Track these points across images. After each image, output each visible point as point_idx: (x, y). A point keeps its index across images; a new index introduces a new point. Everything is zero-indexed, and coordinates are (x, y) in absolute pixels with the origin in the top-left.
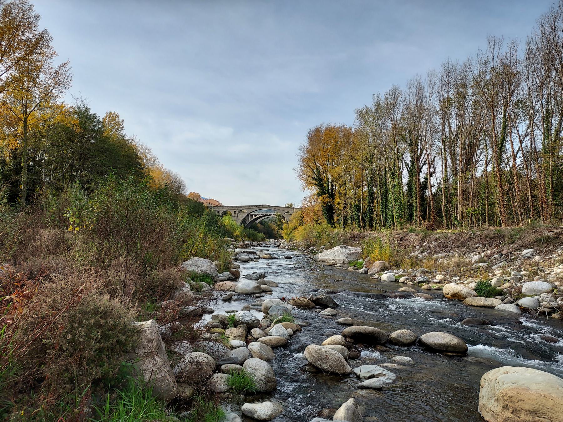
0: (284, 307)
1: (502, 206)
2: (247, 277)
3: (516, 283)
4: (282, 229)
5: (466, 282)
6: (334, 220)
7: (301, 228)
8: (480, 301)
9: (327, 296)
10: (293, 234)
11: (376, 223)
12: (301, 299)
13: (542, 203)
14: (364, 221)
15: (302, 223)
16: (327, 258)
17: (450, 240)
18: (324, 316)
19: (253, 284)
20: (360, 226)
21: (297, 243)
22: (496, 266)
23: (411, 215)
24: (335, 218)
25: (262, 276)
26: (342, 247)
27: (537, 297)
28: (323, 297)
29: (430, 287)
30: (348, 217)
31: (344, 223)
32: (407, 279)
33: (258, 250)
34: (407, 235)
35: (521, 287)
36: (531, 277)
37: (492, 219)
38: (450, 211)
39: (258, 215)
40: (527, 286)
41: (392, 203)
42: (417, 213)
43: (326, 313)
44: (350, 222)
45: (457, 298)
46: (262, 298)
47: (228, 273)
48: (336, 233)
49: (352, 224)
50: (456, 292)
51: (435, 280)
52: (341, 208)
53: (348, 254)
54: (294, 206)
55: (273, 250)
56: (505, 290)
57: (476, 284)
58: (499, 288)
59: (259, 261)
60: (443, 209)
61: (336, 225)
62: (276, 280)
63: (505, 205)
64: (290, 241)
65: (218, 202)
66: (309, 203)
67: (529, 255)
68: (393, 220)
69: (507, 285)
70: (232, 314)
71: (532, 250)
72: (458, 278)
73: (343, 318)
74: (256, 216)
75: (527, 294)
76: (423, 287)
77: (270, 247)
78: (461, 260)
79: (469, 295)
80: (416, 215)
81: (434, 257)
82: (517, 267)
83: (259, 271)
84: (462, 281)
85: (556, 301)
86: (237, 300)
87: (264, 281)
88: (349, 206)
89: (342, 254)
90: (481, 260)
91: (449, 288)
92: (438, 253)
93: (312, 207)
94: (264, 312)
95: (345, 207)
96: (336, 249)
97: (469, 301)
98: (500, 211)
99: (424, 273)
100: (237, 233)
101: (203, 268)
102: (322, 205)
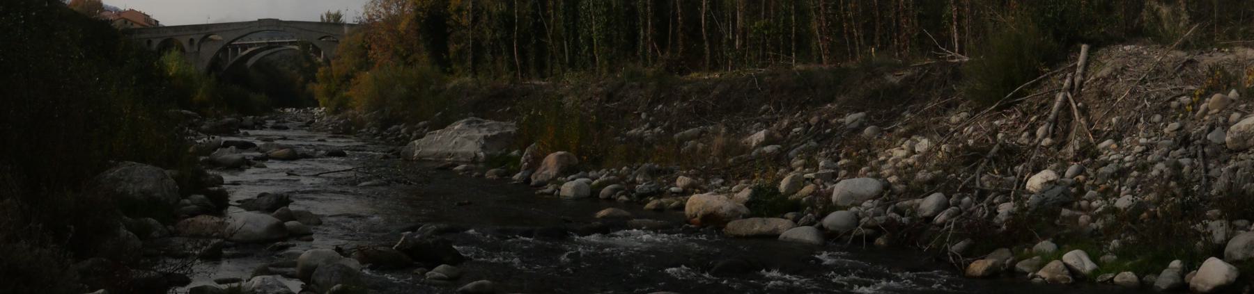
0: (344, 266)
1: (822, 18)
2: (247, 205)
3: (826, 184)
4: (315, 80)
5: (734, 189)
6: (447, 53)
7: (366, 76)
8: (753, 225)
9: (438, 237)
10: (345, 94)
11: (553, 58)
12: (379, 249)
13: (898, 13)
14: (523, 54)
15: (366, 63)
16: (434, 150)
17: (711, 97)
18: (438, 281)
19: (264, 221)
20: (512, 67)
21: (355, 116)
22: (794, 151)
23: (633, 37)
24: (453, 48)
25: (282, 201)
26: (469, 123)
27: (854, 209)
28: (430, 241)
29: (661, 204)
30: (484, 45)
31: (476, 60)
32: (616, 190)
33: (260, 137)
34: (623, 85)
35: (830, 193)
36: (852, 171)
37: (802, 45)
38: (718, 29)
39: (251, 45)
40: (840, 189)
41: (589, 6)
42: (646, 33)
43: (437, 274)
44: (488, 56)
45: (713, 220)
46: (291, 250)
47: (202, 196)
48: (454, 88)
49: (494, 62)
50: (709, 210)
51: (673, 189)
52: (466, 21)
53: (485, 138)
54: (343, 19)
55: (295, 137)
56: (804, 199)
57: (751, 190)
58: (794, 197)
59: (265, 164)
60: (703, 22)
61: (454, 66)
62: (319, 207)
63: (829, 14)
64: (336, 112)
65: (147, 17)
66: (382, 10)
67: (855, 125)
68: (591, 50)
69: (809, 188)
70: (235, 285)
71: (861, 114)
72: (721, 181)
73: (475, 283)
75: (840, 204)
76: (648, 206)
77: (286, 128)
78: (731, 140)
79: (735, 215)
80: (645, 38)
81: (676, 136)
82: (833, 150)
83: (270, 190)
84: (728, 188)
85: (885, 213)
86: (233, 256)
87: (289, 211)
88: (486, 17)
89: (471, 138)
90: (769, 140)
91: (698, 203)
92: (686, 128)
93: (392, 22)
94: (302, 280)
95: (475, 20)
96: (456, 127)
97: (734, 227)
98: (820, 29)
99: (653, 173)
100: (200, 95)
101: (145, 187)
102: (418, 16)
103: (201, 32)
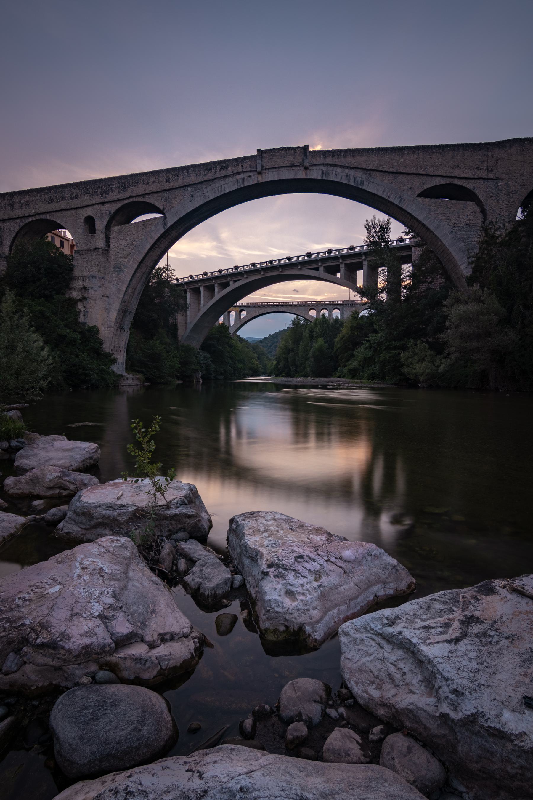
74: (227, 285)
103: (110, 197)
